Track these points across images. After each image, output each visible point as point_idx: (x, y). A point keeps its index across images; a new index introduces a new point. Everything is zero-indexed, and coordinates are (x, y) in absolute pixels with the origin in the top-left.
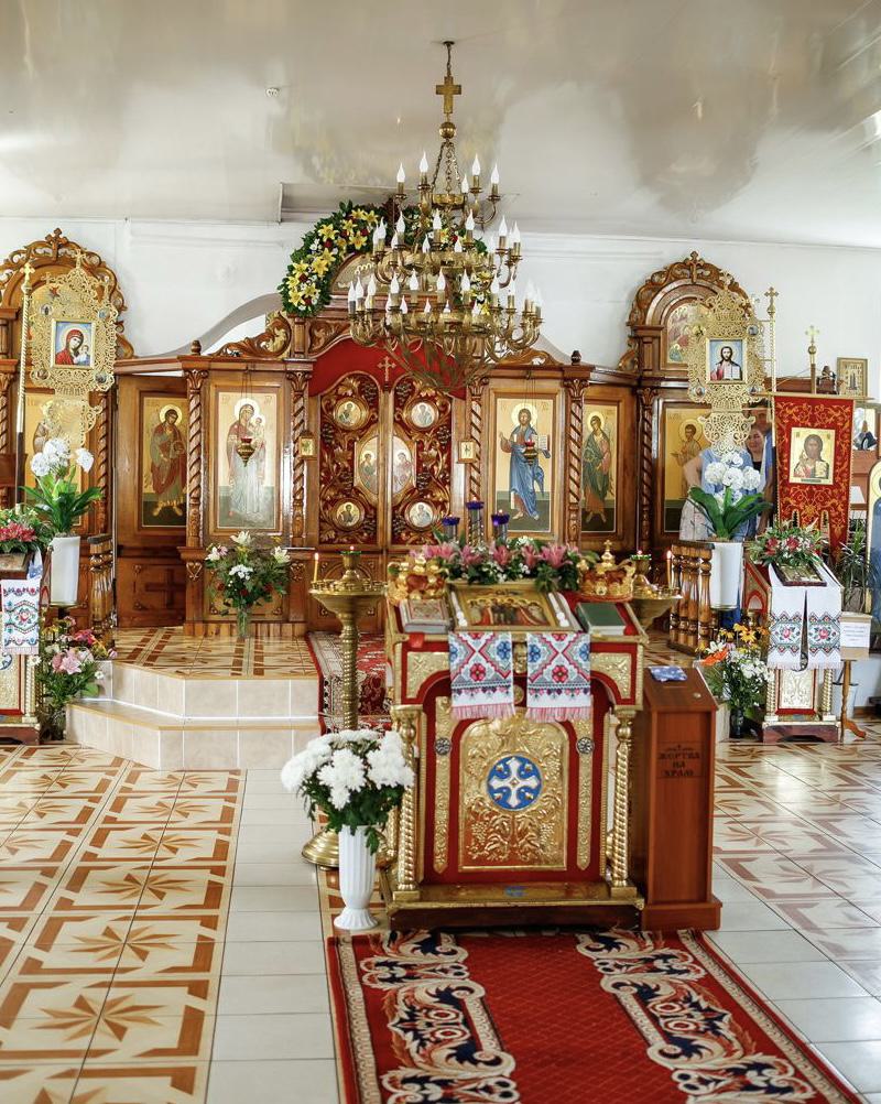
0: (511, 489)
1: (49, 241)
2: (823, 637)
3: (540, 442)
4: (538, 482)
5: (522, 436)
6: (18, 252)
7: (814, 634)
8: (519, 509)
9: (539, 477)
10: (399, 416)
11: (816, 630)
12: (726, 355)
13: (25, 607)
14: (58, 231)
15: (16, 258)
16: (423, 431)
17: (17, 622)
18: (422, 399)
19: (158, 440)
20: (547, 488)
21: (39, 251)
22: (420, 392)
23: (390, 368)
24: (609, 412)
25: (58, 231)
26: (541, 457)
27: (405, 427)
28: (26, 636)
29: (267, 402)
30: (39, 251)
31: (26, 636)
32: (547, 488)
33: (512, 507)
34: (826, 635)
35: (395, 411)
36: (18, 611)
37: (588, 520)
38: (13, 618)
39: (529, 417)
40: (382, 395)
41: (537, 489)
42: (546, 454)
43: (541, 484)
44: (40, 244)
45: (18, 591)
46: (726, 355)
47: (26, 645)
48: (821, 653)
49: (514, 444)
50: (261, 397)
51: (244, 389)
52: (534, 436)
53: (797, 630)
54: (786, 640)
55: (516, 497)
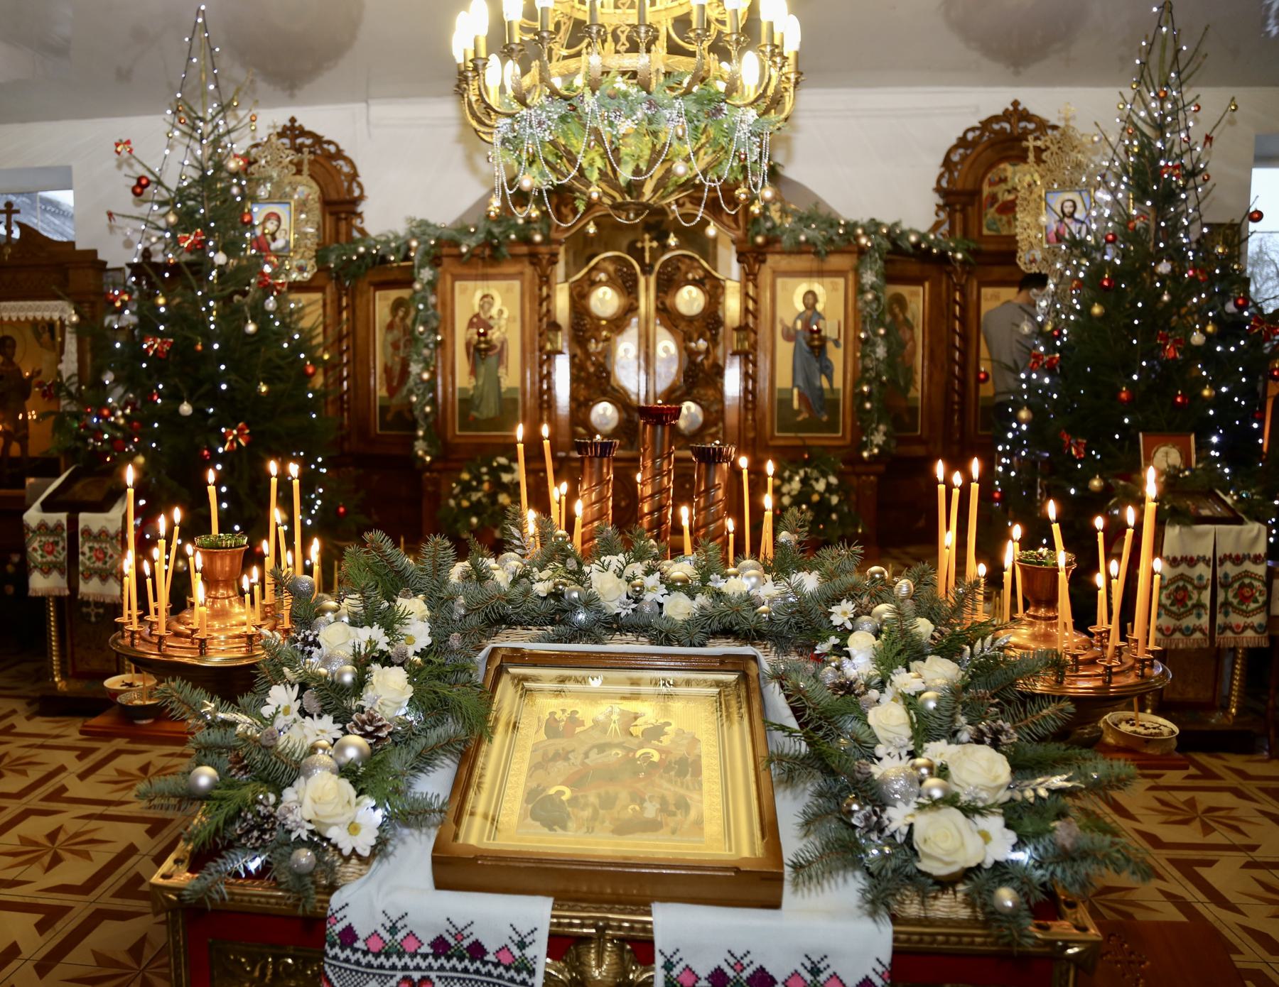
0: (794, 385)
1: (1006, 116)
2: (98, 559)
3: (830, 328)
4: (827, 376)
5: (807, 324)
6: (973, 129)
7: (88, 554)
8: (803, 409)
9: (827, 370)
10: (663, 303)
11: (91, 549)
12: (1068, 209)
13: (1247, 581)
14: (293, 120)
15: (970, 136)
16: (690, 320)
17: (1235, 602)
18: (689, 283)
19: (390, 338)
20: (838, 382)
21: (996, 127)
22: (687, 273)
23: (651, 248)
24: (509, 290)
25: (293, 120)
26: (830, 345)
27: (668, 316)
28: (1249, 620)
29: (509, 290)
30: (996, 127)
31: (1249, 620)
32: (838, 382)
33: (796, 404)
34: (102, 555)
35: (657, 298)
36: (1236, 585)
37: (389, 417)
38: (1195, 596)
39: (816, 300)
40: (642, 280)
41: (825, 384)
42: (836, 343)
43: (830, 380)
44: (995, 119)
45: (1237, 557)
46: (1068, 209)
47: (1249, 633)
48: (95, 582)
49: (797, 331)
50: (503, 284)
51: (485, 277)
52: (821, 323)
53: (61, 544)
54: (50, 558)
55: (801, 395)
